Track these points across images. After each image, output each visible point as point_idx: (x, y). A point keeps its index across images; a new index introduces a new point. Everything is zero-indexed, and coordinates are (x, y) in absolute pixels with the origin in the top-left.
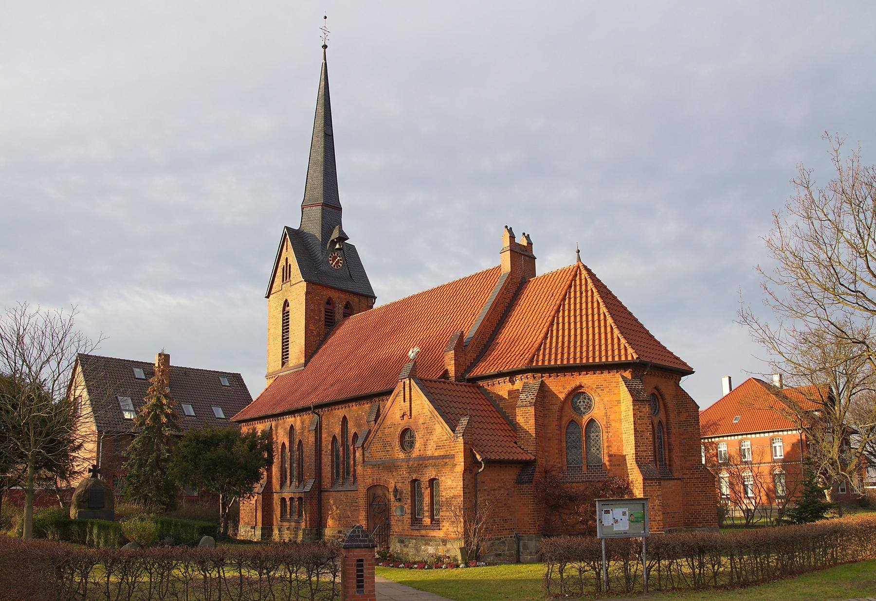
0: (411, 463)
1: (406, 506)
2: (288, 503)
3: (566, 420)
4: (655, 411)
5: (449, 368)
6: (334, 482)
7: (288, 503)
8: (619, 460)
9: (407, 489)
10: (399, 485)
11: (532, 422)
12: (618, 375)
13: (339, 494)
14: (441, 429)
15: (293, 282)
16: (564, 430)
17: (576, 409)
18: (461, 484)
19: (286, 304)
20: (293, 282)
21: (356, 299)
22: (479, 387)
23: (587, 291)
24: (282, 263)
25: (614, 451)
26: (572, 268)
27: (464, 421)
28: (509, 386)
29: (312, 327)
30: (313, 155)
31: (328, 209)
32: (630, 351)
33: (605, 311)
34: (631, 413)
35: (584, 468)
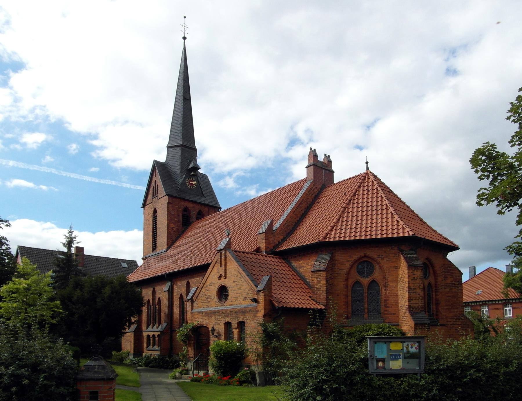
2: (151, 338)
4: (425, 275)
7: (151, 338)
16: (350, 288)
19: (155, 211)
20: (160, 197)
24: (153, 184)
29: (172, 225)
31: (186, 149)
32: (407, 229)
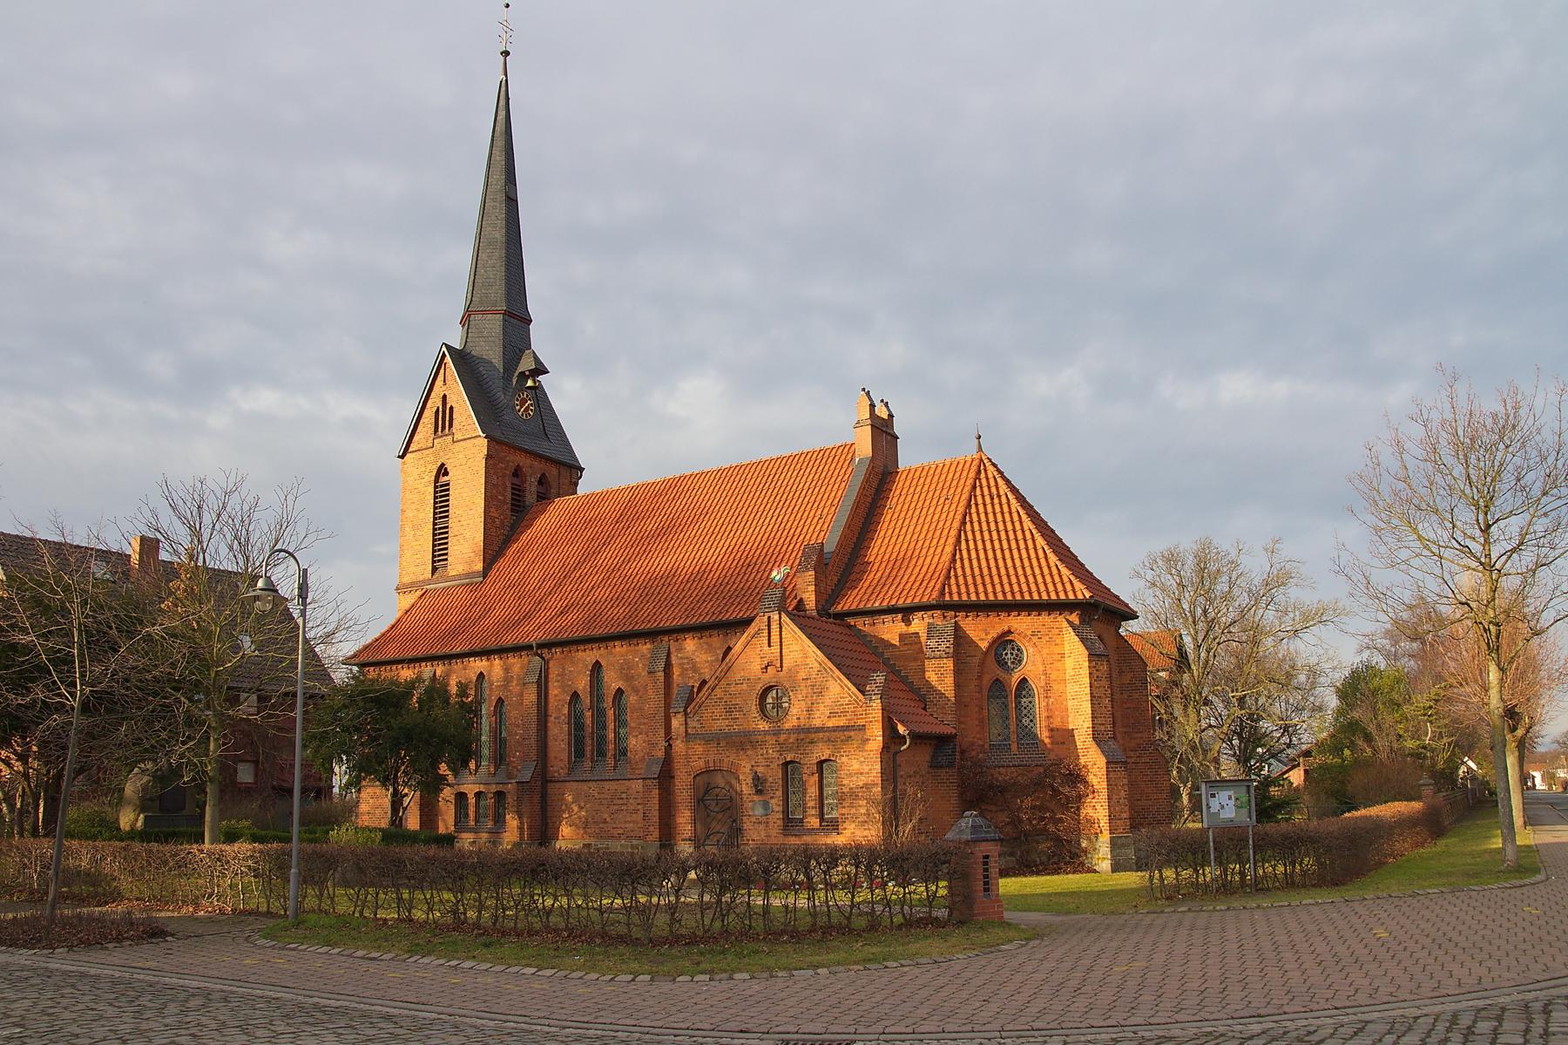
0: (783, 737)
1: (773, 801)
3: (993, 678)
5: (805, 596)
6: (572, 768)
8: (1065, 737)
9: (774, 776)
10: (760, 770)
11: (950, 680)
12: (1061, 618)
13: (585, 786)
14: (839, 689)
15: (458, 436)
16: (985, 692)
17: (1002, 663)
18: (878, 767)
19: (442, 471)
20: (458, 436)
21: (554, 471)
22: (849, 626)
23: (999, 496)
24: (435, 402)
25: (1056, 723)
26: (969, 459)
27: (880, 678)
28: (901, 627)
30: (487, 230)
32: (1078, 585)
33: (1032, 527)
34: (1085, 671)
35: (1014, 747)
